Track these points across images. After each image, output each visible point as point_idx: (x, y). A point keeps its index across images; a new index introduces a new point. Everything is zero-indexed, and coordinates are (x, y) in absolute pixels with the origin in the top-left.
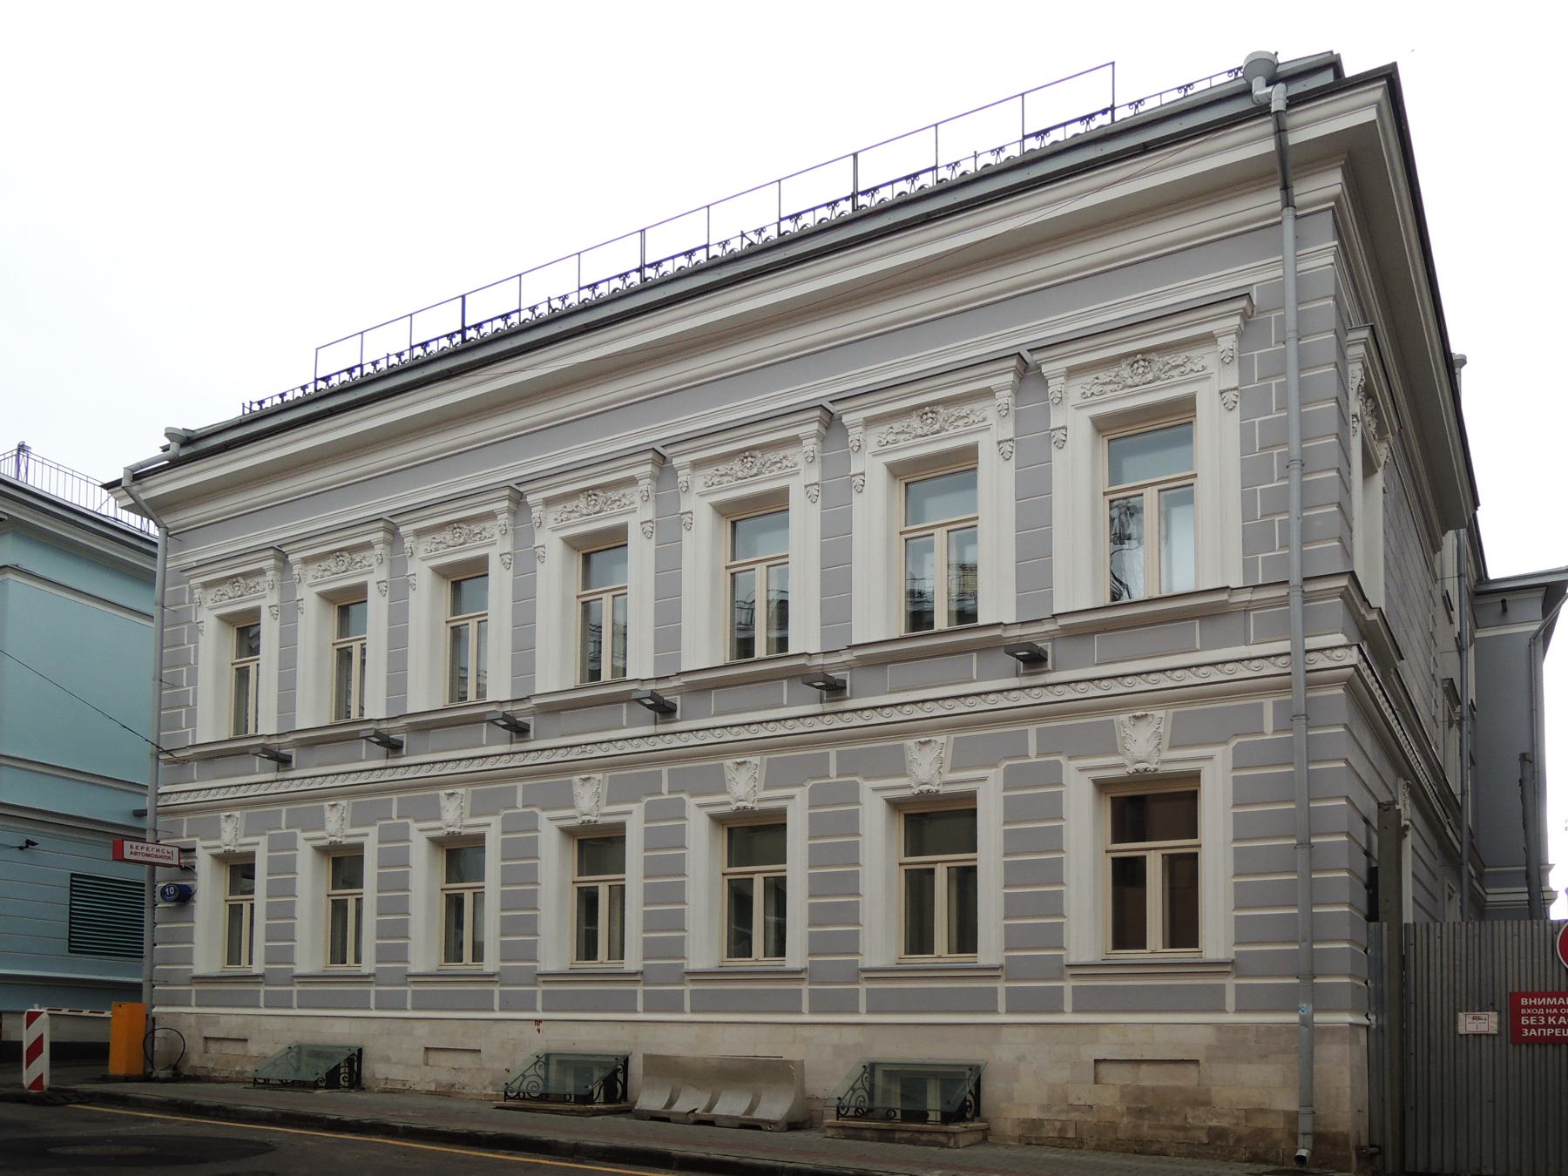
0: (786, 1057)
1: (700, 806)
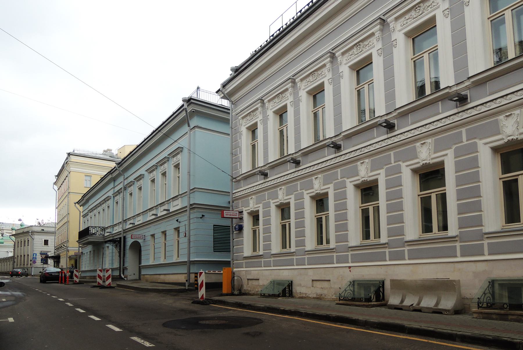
0: (451, 279)
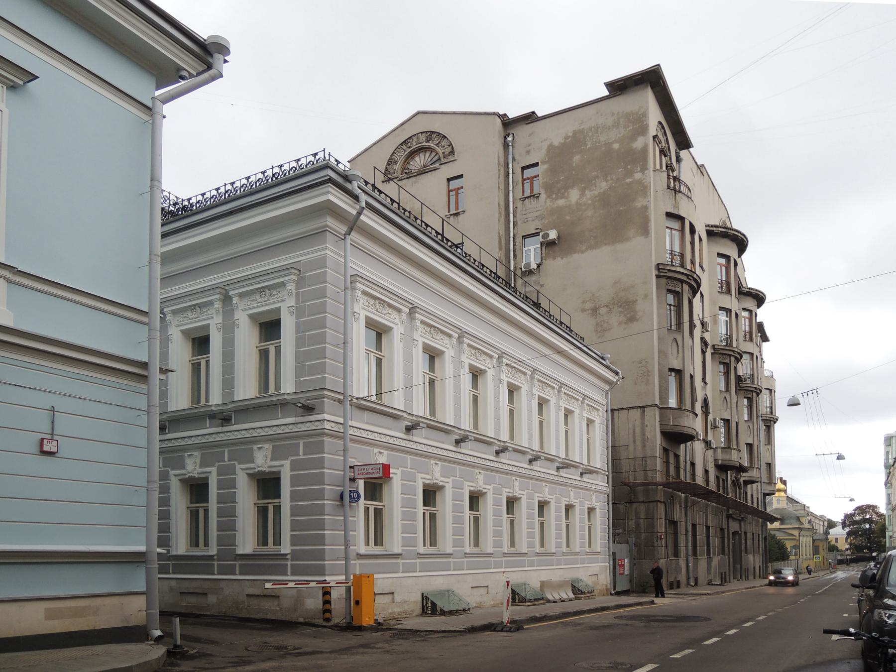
1: (243, 469)
